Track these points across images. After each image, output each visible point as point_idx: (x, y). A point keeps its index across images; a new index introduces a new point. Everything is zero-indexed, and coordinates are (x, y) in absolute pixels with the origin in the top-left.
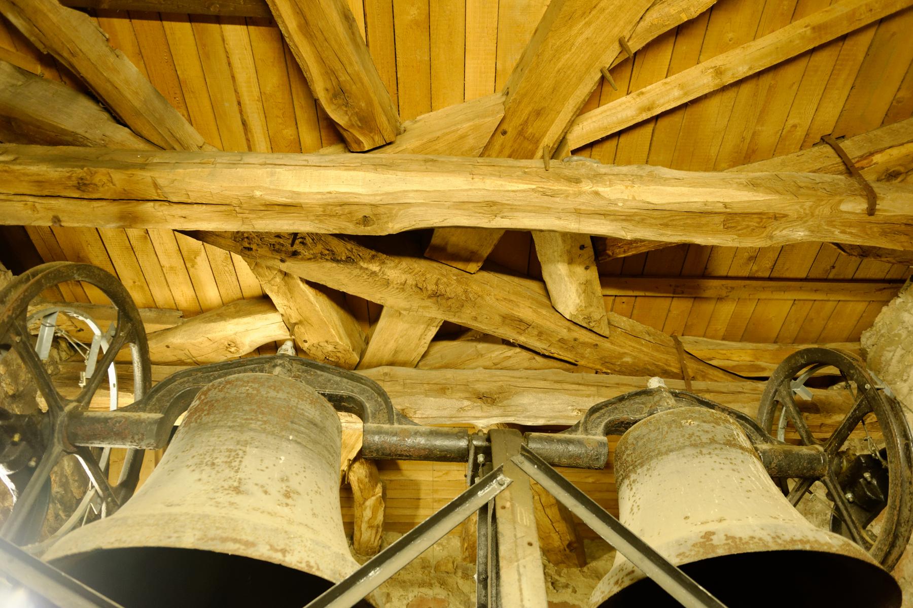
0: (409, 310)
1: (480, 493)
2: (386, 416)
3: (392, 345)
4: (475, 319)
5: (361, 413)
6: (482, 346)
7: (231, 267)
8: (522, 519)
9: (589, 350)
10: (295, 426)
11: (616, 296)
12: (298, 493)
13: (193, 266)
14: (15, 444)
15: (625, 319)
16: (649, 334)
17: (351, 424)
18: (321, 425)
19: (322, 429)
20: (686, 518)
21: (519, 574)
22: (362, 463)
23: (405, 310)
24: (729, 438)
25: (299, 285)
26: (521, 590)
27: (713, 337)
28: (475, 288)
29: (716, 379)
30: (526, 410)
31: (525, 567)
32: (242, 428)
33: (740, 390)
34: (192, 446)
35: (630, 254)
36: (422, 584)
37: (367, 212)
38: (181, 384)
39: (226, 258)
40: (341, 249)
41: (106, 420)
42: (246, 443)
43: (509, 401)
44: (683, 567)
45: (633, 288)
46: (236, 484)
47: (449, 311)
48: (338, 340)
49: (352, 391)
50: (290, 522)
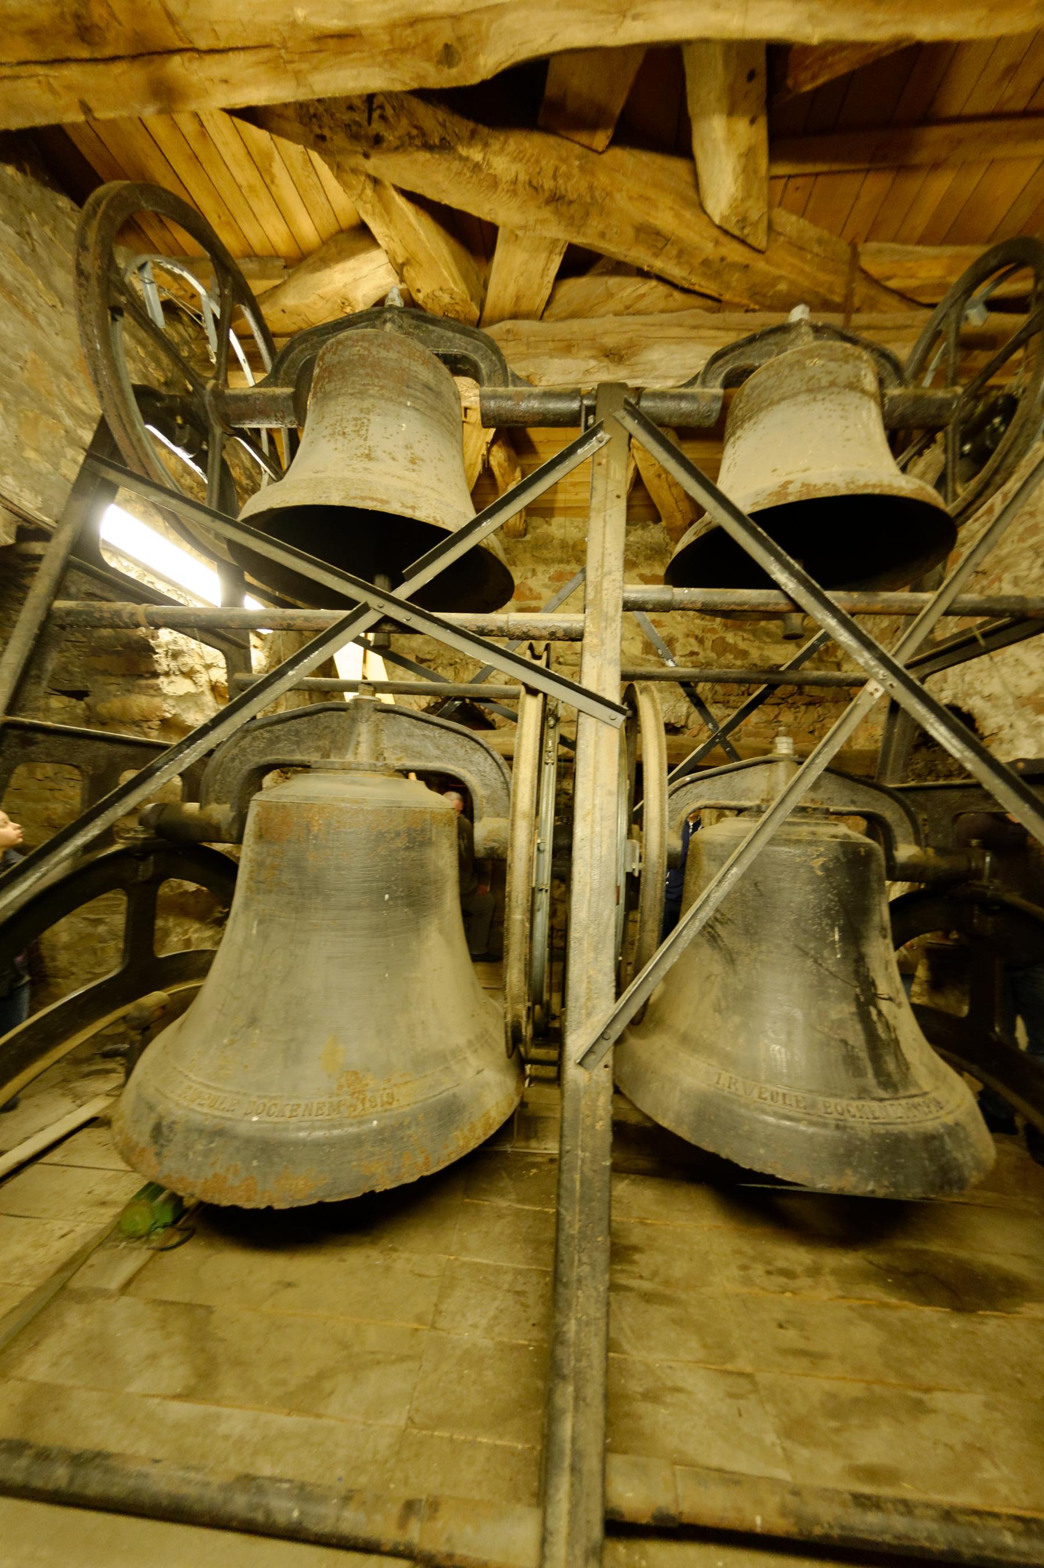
0: (524, 228)
1: (580, 451)
2: (501, 377)
3: (512, 289)
4: (603, 235)
5: (476, 375)
6: (613, 281)
7: (316, 179)
9: (737, 275)
10: (411, 391)
11: (790, 177)
12: (423, 460)
13: (273, 182)
14: (181, 427)
15: (794, 218)
17: (468, 391)
18: (436, 389)
19: (438, 395)
20: (774, 470)
21: (605, 522)
22: (500, 446)
23: (521, 228)
25: (393, 198)
26: (604, 534)
27: (905, 241)
28: (602, 179)
30: (654, 369)
32: (361, 394)
33: (909, 322)
34: (323, 417)
35: (820, 81)
36: (561, 561)
37: (445, 35)
38: (301, 351)
39: (305, 160)
40: (430, 118)
41: (246, 398)
42: (368, 411)
44: (752, 515)
45: (814, 159)
46: (366, 452)
47: (572, 225)
48: (452, 286)
49: (466, 349)
50: (417, 485)
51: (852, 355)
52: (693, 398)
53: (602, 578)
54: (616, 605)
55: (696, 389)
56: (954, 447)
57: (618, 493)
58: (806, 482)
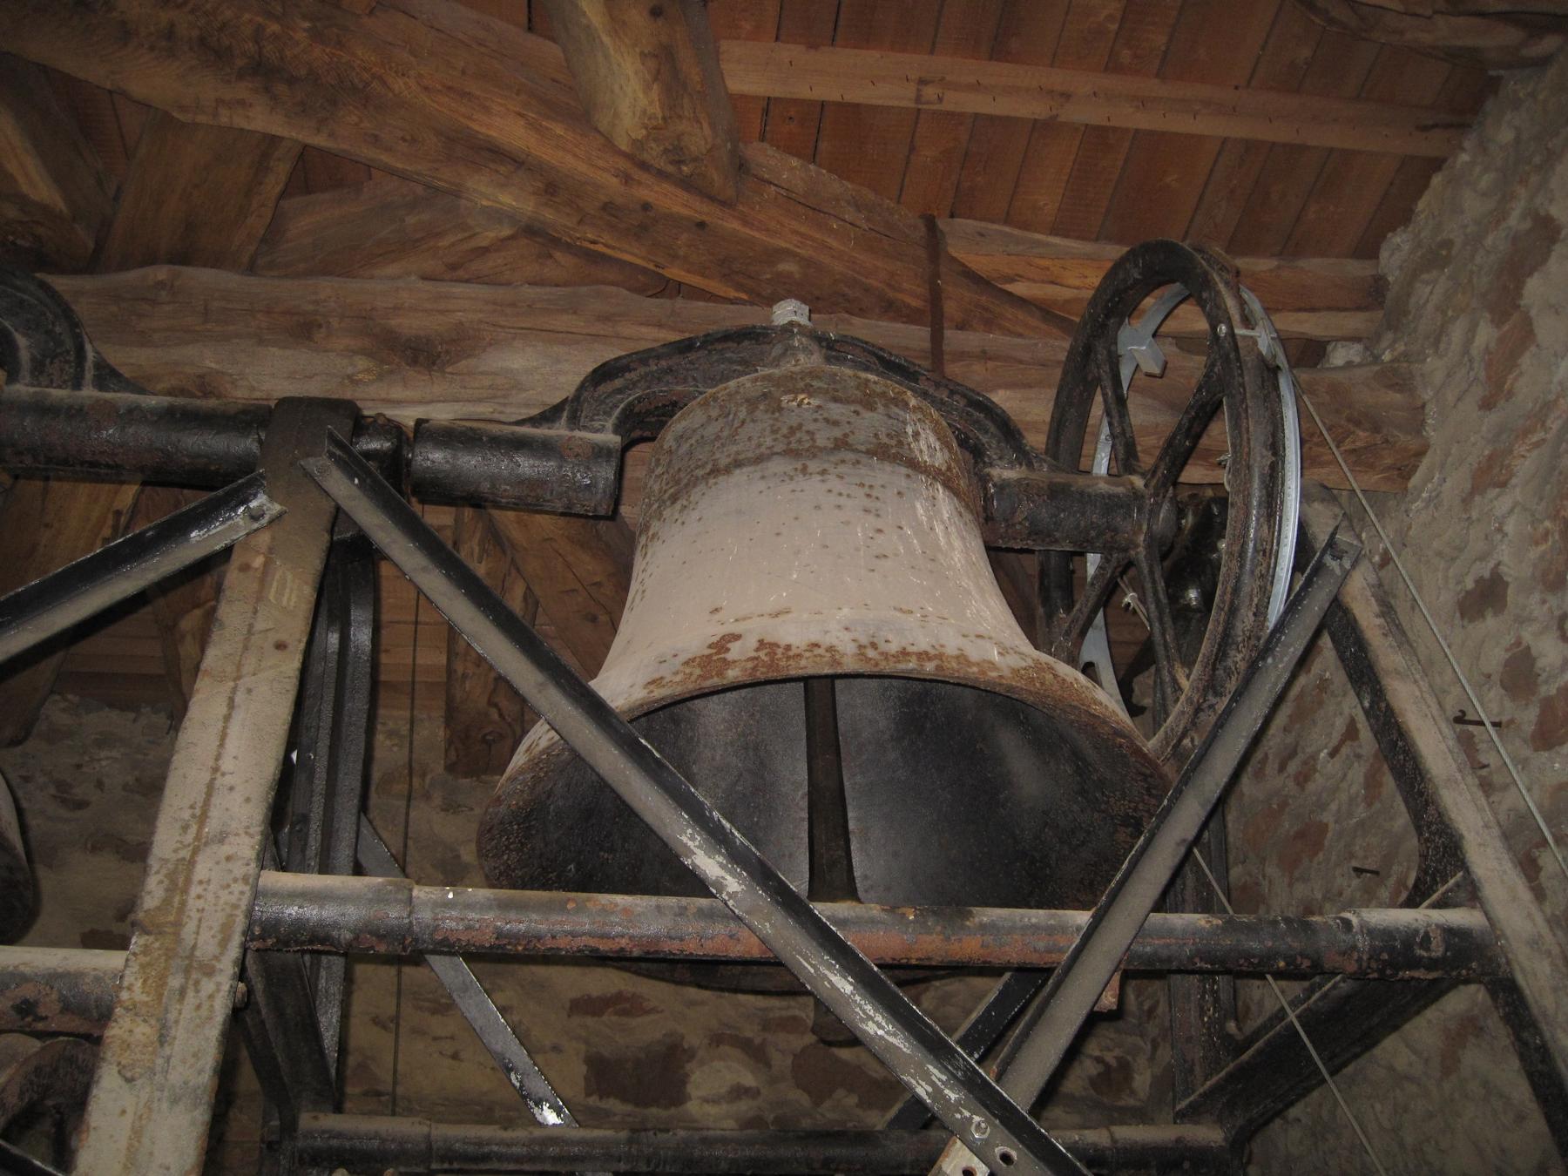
8: (280, 593)
9: (685, 237)
15: (795, 162)
16: (858, 208)
21: (231, 704)
24: (885, 440)
29: (1020, 330)
31: (249, 691)
43: (472, 362)
51: (883, 394)
52: (545, 448)
53: (196, 851)
54: (226, 929)
55: (558, 431)
56: (1155, 593)
57: (282, 636)
58: (768, 639)
